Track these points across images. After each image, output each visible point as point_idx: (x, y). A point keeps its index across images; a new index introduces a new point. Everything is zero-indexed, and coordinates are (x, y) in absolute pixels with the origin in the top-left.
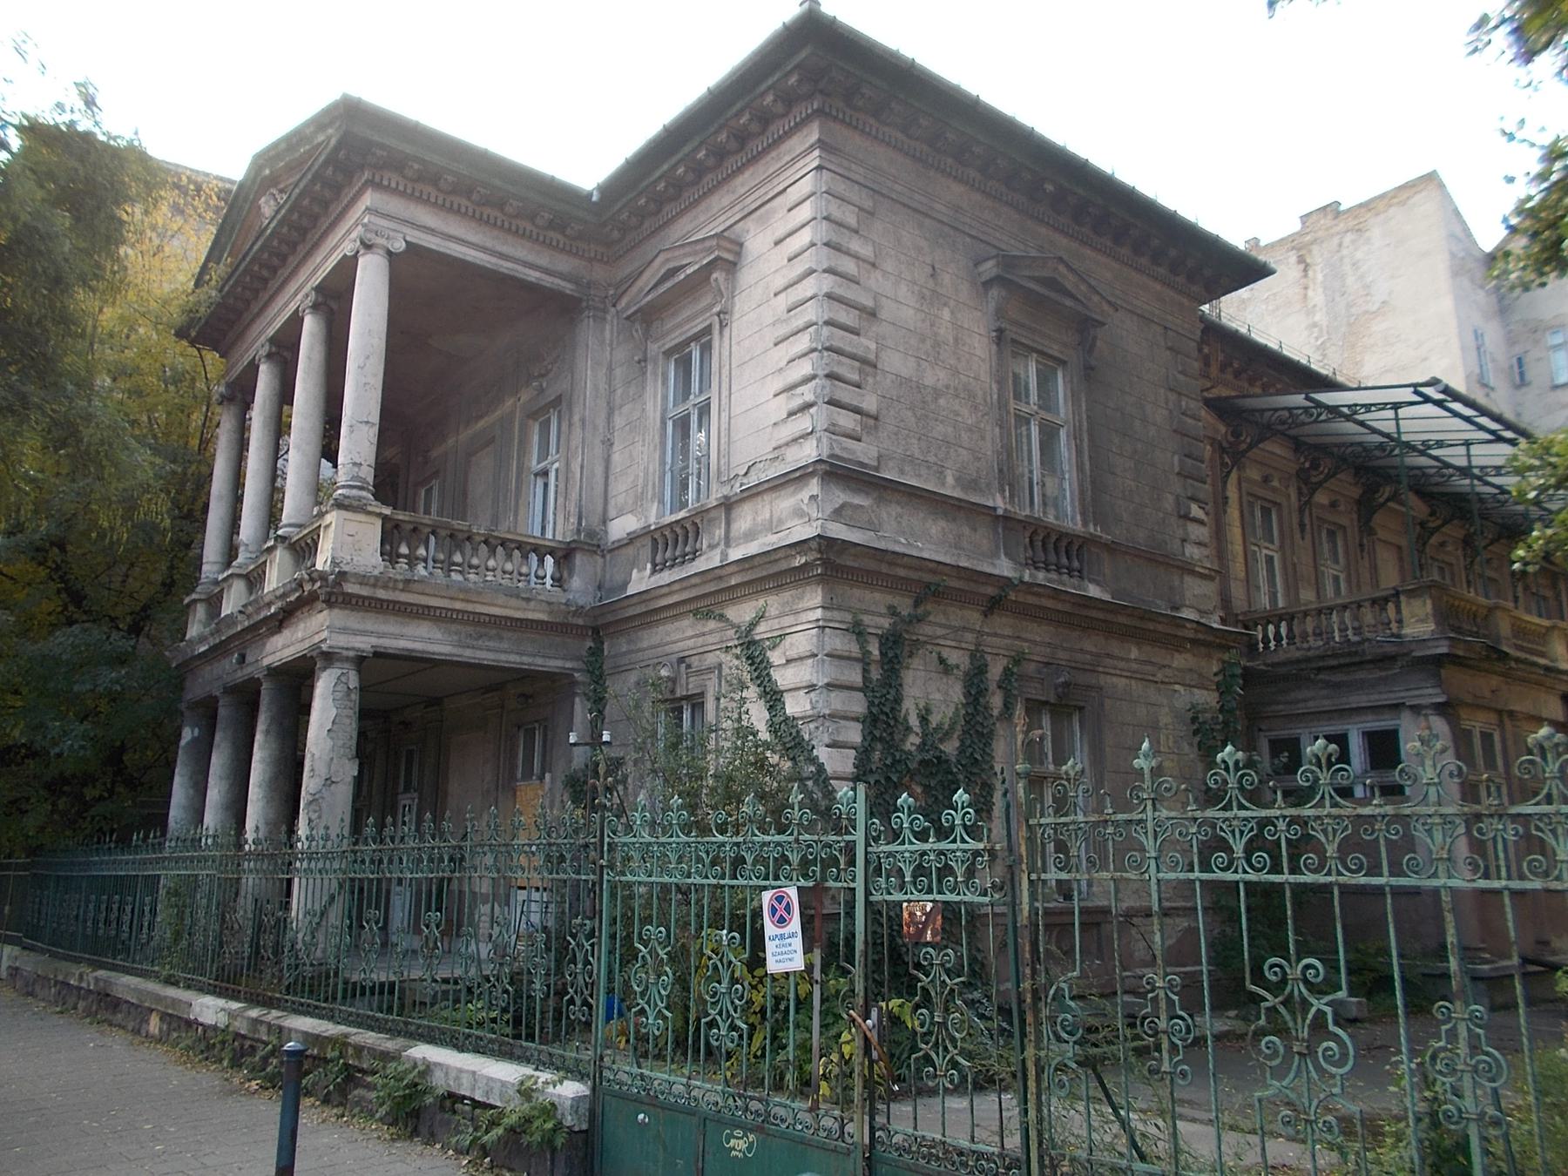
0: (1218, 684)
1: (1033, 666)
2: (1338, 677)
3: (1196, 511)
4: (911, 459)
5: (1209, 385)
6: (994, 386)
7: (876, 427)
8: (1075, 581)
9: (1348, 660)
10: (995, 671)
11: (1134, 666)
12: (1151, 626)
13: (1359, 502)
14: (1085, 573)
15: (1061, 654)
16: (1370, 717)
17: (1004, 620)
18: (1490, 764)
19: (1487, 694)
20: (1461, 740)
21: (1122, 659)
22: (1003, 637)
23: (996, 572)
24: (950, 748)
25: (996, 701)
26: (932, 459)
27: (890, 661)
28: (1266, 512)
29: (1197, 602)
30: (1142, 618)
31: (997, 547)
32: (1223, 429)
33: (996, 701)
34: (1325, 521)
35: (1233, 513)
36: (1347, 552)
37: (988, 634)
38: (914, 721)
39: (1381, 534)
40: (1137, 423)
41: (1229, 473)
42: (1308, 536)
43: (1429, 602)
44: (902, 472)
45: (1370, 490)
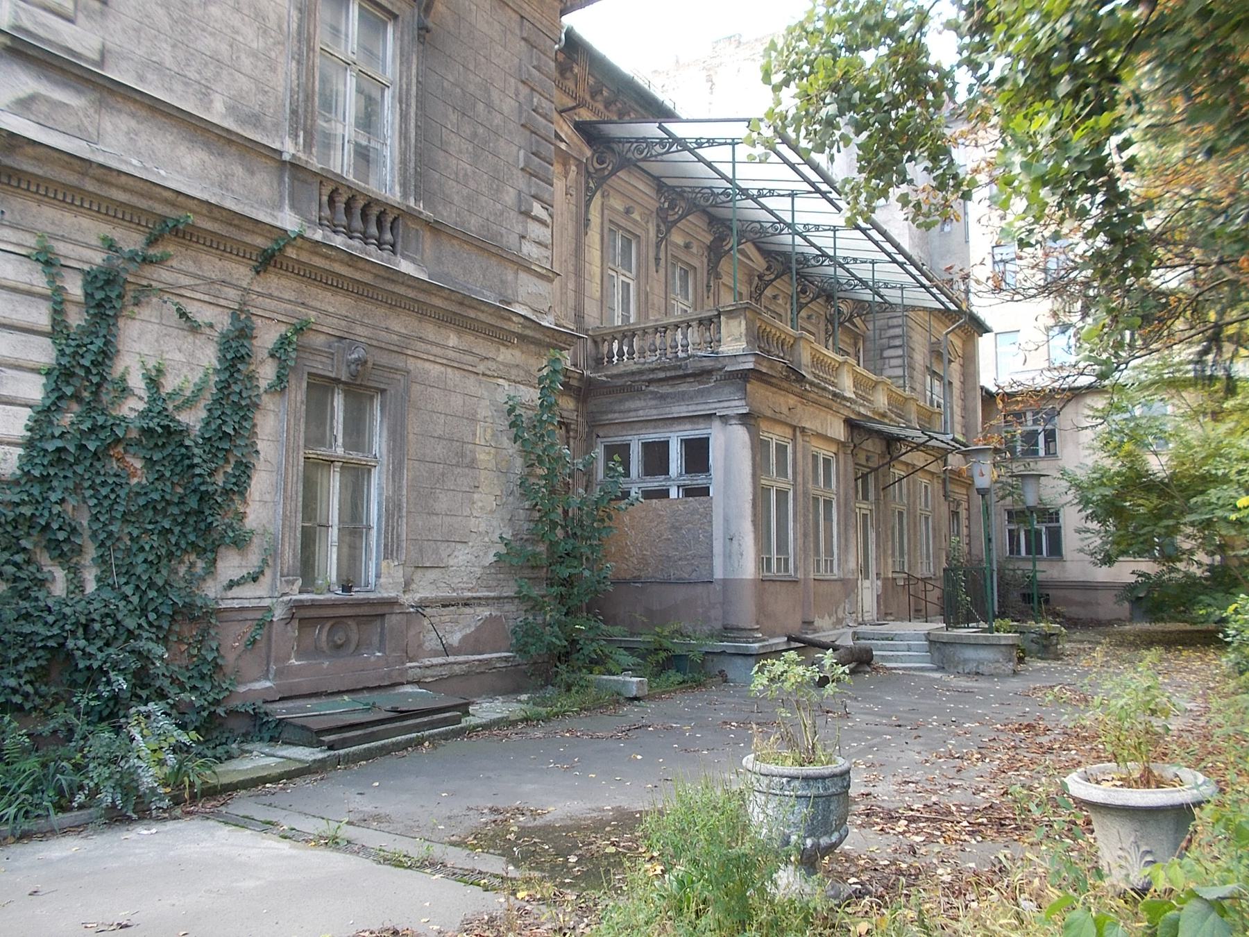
0: (541, 381)
1: (322, 338)
2: (665, 389)
3: (537, 209)
4: (159, 67)
5: (571, 104)
6: (295, 14)
7: (102, 14)
8: (385, 254)
9: (673, 373)
10: (267, 337)
11: (451, 354)
12: (472, 314)
13: (710, 248)
14: (399, 247)
15: (359, 330)
16: (688, 426)
17: (284, 281)
18: (782, 471)
19: (785, 410)
20: (759, 447)
21: (437, 345)
22: (280, 299)
23: (279, 224)
24: (193, 419)
25: (266, 372)
26: (193, 75)
27: (99, 305)
28: (627, 244)
29: (533, 299)
30: (461, 304)
31: (282, 197)
32: (588, 153)
33: (266, 372)
34: (680, 260)
35: (594, 236)
36: (695, 289)
37: (259, 294)
38: (136, 382)
39: (726, 279)
40: (481, 107)
41: (591, 198)
42: (662, 271)
43: (743, 323)
44: (141, 79)
45: (720, 239)
